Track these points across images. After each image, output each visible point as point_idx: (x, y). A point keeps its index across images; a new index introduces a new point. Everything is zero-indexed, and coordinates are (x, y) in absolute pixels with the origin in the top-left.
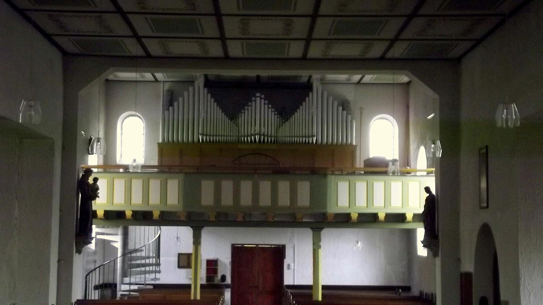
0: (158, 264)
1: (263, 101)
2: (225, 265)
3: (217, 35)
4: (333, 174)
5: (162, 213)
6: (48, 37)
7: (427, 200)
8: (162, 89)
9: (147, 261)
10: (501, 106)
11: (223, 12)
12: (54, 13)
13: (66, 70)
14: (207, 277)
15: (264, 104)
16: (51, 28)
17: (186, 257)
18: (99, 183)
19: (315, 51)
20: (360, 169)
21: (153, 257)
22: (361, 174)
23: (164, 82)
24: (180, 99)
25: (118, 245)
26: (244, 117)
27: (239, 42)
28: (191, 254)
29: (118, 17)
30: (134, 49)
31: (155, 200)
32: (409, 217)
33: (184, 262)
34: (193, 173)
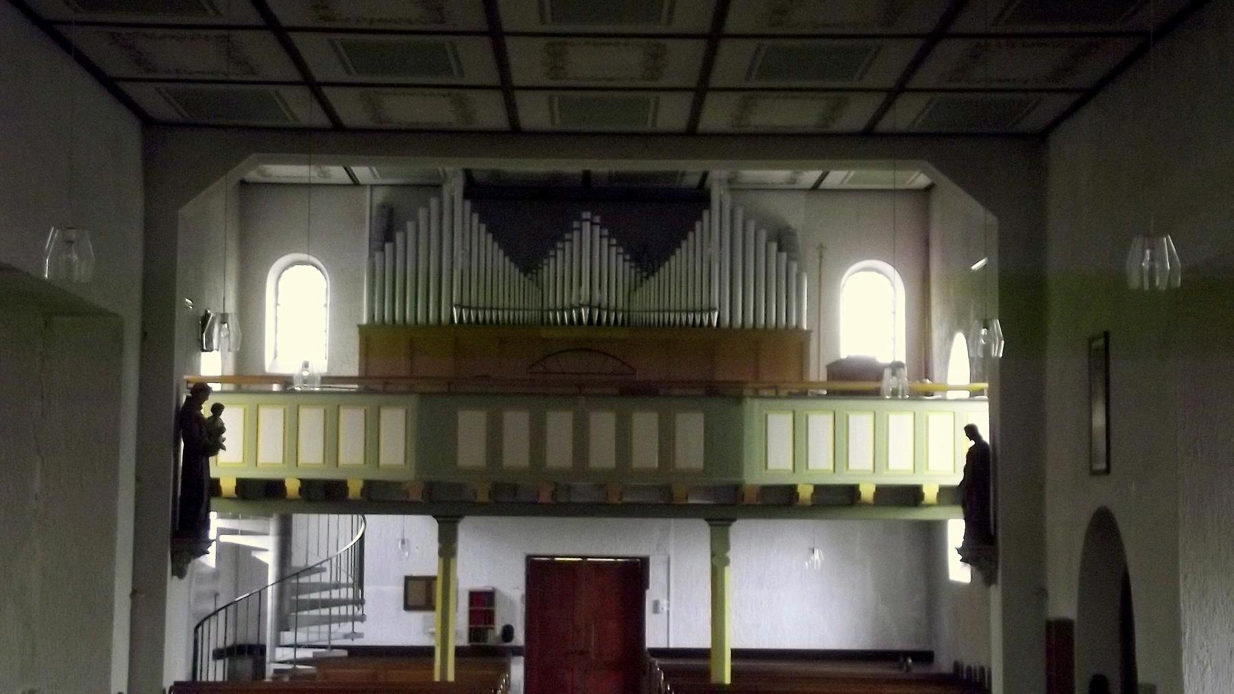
0: (359, 602)
1: (597, 229)
2: (512, 603)
3: (494, 79)
4: (757, 395)
5: (369, 485)
6: (110, 84)
7: (971, 455)
8: (368, 202)
9: (335, 594)
10: (1138, 242)
12: (124, 31)
13: (149, 158)
14: (471, 630)
15: (601, 237)
16: (116, 63)
17: (422, 585)
18: (224, 417)
19: (716, 116)
20: (818, 385)
21: (347, 586)
22: (820, 397)
23: (372, 186)
24: (410, 226)
25: (269, 557)
26: (555, 267)
27: (542, 97)
28: (434, 579)
29: (268, 38)
30: (305, 112)
31: (351, 454)
32: (930, 493)
33: (418, 596)
34: (439, 394)
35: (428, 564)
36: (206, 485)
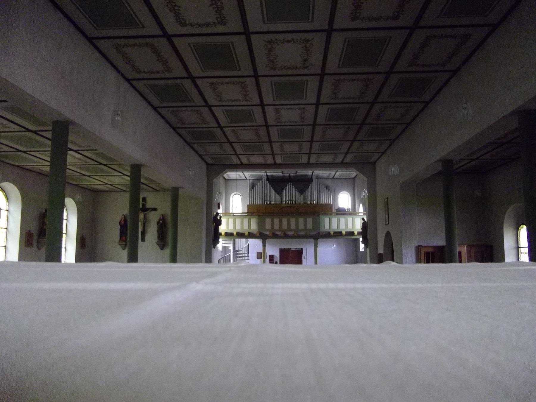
0: (248, 256)
1: (292, 186)
2: (277, 257)
3: (268, 140)
4: (323, 214)
5: (249, 233)
6: (200, 156)
7: (363, 223)
8: (249, 183)
9: (244, 255)
10: (391, 166)
11: (265, 103)
12: (203, 144)
13: (207, 169)
14: (269, 259)
15: (294, 189)
16: (202, 152)
17: (260, 254)
18: (222, 219)
19: (313, 160)
20: (334, 213)
21: (246, 254)
22: (334, 215)
23: (249, 179)
24: (256, 186)
25: (231, 248)
26: (284, 193)
27: (279, 156)
28: (261, 253)
29: (228, 145)
30: (236, 161)
31: (246, 227)
32: (356, 233)
33: (259, 256)
34: (263, 215)
35: (261, 251)
36: (219, 234)
